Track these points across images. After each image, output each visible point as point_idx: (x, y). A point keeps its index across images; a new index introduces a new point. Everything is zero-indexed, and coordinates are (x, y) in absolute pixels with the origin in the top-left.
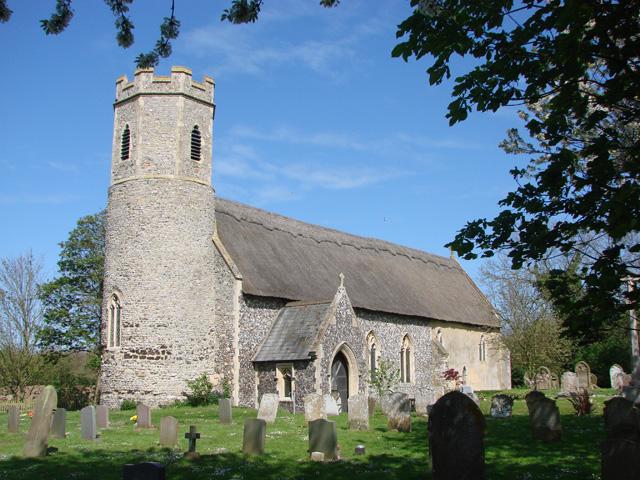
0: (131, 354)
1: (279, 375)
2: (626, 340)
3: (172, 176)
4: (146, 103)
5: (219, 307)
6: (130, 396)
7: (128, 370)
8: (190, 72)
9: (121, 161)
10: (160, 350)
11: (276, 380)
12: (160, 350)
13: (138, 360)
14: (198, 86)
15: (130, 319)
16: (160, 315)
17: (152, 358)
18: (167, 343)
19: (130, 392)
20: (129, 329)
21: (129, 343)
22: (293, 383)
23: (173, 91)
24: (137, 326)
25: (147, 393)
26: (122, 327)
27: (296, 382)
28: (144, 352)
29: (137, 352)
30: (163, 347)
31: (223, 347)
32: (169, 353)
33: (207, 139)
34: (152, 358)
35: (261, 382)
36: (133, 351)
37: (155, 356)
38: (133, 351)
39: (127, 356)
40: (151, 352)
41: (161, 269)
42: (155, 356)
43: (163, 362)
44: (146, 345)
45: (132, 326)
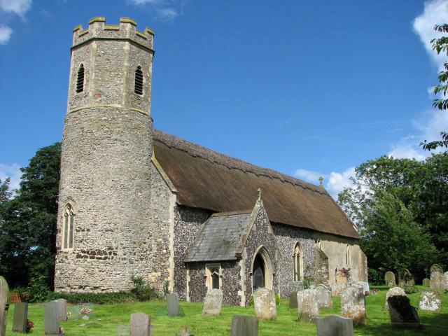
0: (83, 254)
1: (208, 272)
3: (119, 106)
4: (98, 47)
5: (156, 217)
7: (79, 269)
9: (76, 94)
10: (108, 252)
11: (205, 277)
12: (108, 252)
13: (88, 260)
14: (111, 28)
15: (82, 225)
16: (109, 221)
18: (114, 245)
19: (81, 287)
21: (81, 245)
22: (220, 280)
23: (121, 37)
24: (88, 230)
26: (74, 232)
27: (224, 280)
28: (93, 253)
29: (88, 252)
30: (110, 248)
32: (115, 254)
34: (101, 259)
35: (191, 279)
36: (84, 252)
37: (103, 257)
38: (84, 252)
39: (79, 256)
40: (100, 252)
42: (103, 257)
43: (110, 261)
44: (95, 247)
45: (83, 231)
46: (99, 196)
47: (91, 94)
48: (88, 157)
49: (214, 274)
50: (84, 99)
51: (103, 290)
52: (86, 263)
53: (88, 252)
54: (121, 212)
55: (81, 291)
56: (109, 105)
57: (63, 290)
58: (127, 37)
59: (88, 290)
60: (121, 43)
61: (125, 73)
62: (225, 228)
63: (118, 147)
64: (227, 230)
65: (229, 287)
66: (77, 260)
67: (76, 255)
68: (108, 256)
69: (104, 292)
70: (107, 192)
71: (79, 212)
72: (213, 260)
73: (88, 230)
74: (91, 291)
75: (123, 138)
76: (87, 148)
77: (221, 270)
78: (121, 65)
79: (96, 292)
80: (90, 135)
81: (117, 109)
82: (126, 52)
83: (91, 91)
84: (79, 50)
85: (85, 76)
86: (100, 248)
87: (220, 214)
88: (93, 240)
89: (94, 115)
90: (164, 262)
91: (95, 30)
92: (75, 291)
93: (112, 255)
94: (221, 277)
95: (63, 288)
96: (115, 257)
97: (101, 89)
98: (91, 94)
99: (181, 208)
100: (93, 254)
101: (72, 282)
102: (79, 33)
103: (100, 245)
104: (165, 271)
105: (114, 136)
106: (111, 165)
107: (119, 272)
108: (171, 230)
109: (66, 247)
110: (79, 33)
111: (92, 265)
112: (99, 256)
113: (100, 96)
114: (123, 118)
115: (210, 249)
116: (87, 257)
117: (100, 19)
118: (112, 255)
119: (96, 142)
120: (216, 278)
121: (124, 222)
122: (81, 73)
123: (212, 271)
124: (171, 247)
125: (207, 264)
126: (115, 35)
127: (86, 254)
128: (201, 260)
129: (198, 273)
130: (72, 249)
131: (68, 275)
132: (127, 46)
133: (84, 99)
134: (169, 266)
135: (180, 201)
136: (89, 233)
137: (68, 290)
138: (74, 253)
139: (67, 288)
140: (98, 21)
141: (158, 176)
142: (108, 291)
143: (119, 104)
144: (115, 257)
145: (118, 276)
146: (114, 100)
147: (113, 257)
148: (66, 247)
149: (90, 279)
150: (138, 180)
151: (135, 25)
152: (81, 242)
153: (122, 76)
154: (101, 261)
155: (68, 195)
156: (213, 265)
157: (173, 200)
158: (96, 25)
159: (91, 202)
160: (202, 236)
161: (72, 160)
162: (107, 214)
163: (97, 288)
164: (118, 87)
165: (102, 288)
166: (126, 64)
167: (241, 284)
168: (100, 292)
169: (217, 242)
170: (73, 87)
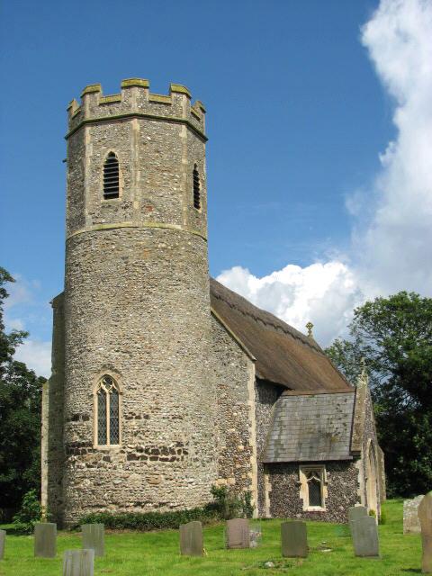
0: (139, 454)
1: (303, 479)
2: (36, 503)
3: (179, 227)
4: (142, 129)
5: (223, 396)
6: (138, 509)
7: (135, 476)
8: (147, 84)
9: (103, 200)
10: (176, 449)
11: (300, 484)
12: (176, 449)
13: (148, 462)
14: (159, 100)
15: (135, 408)
16: (176, 403)
17: (166, 460)
18: (184, 440)
19: (138, 504)
20: (134, 422)
21: (136, 440)
22: (325, 490)
23: (174, 117)
24: (147, 417)
25: (162, 504)
26: (122, 420)
27: (330, 489)
28: (156, 452)
29: (147, 451)
30: (179, 444)
31: (232, 443)
32: (186, 453)
33: (203, 181)
34: (166, 460)
35: (274, 487)
36: (141, 451)
37: (170, 457)
38: (141, 451)
39: (131, 457)
40: (165, 451)
41: (173, 345)
42: (170, 457)
43: (180, 463)
44: (159, 442)
45: (138, 417)
46: (161, 365)
47: (136, 205)
48: (140, 304)
49: (313, 480)
50: (121, 212)
51: (171, 507)
52: (145, 467)
53: (147, 451)
54: (190, 389)
55: (138, 509)
56: (167, 226)
57: (103, 510)
58: (184, 117)
59: (150, 508)
60: (175, 126)
61: (184, 175)
62: (315, 413)
63: (182, 291)
64: (318, 416)
65: (339, 499)
66: (128, 463)
67: (126, 455)
68: (177, 456)
69: (174, 510)
70: (172, 360)
71: (129, 389)
72: (313, 460)
73: (147, 417)
74: (155, 510)
75: (187, 277)
76: (137, 290)
77: (326, 473)
78: (177, 162)
79: (163, 510)
80: (141, 271)
81: (178, 231)
82: (184, 142)
83: (135, 199)
84: (100, 128)
85: (121, 176)
86: (165, 443)
87: (297, 392)
88: (156, 433)
89: (145, 240)
90: (241, 463)
91: (134, 100)
92: (129, 510)
93: (182, 454)
94: (326, 484)
95: (101, 506)
96: (185, 457)
97: (151, 198)
98: (136, 205)
99: (260, 383)
100: (154, 453)
101: (122, 495)
102: (99, 98)
103: (165, 439)
104: (244, 477)
105: (177, 274)
106: (175, 319)
107: (191, 480)
108: (252, 418)
109: (102, 441)
110: (99, 98)
111: (155, 469)
112: (164, 456)
113: (150, 209)
114: (186, 246)
115: (300, 444)
116: (146, 458)
117: (141, 82)
118: (182, 454)
119: (152, 282)
120: (315, 488)
121: (195, 406)
122: (111, 168)
123: (308, 477)
124: (253, 442)
125: (300, 466)
126: (164, 113)
127: (144, 454)
128: (293, 459)
129: (286, 480)
130: (117, 447)
131: (112, 487)
132: (184, 132)
133: (121, 212)
134: (250, 469)
135: (262, 374)
136: (148, 421)
137: (113, 510)
138: (122, 452)
139: (113, 506)
140: (139, 86)
141: (224, 335)
142: (179, 509)
143: (178, 224)
144: (185, 457)
145: (189, 485)
146: (172, 217)
147: (182, 458)
148: (102, 441)
149: (153, 493)
150: (205, 342)
151: (147, 88)
152: (135, 435)
153: (180, 180)
154: (168, 463)
155: (106, 362)
156: (312, 467)
157: (252, 371)
158: (136, 92)
159: (150, 375)
160: (277, 424)
161: (109, 307)
162: (174, 392)
163: (164, 504)
164: (175, 196)
165: (172, 504)
166: (184, 161)
167: (359, 495)
168: (168, 510)
169: (309, 433)
170: (95, 188)
